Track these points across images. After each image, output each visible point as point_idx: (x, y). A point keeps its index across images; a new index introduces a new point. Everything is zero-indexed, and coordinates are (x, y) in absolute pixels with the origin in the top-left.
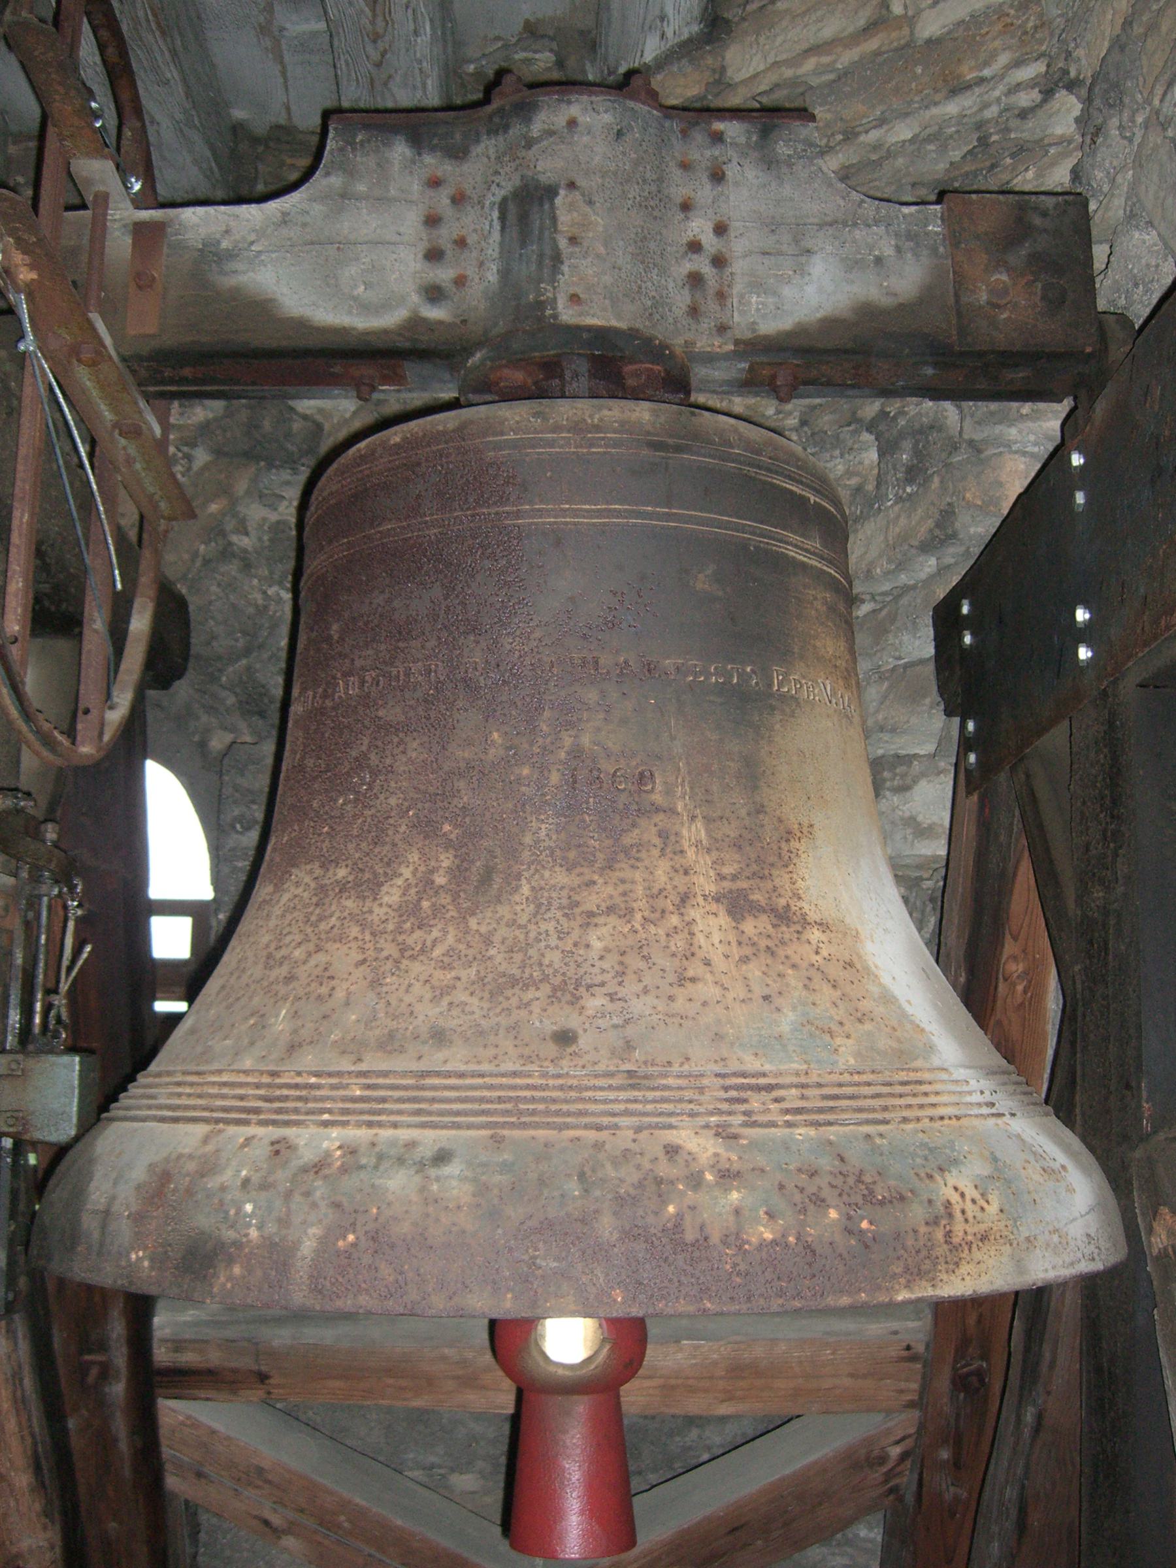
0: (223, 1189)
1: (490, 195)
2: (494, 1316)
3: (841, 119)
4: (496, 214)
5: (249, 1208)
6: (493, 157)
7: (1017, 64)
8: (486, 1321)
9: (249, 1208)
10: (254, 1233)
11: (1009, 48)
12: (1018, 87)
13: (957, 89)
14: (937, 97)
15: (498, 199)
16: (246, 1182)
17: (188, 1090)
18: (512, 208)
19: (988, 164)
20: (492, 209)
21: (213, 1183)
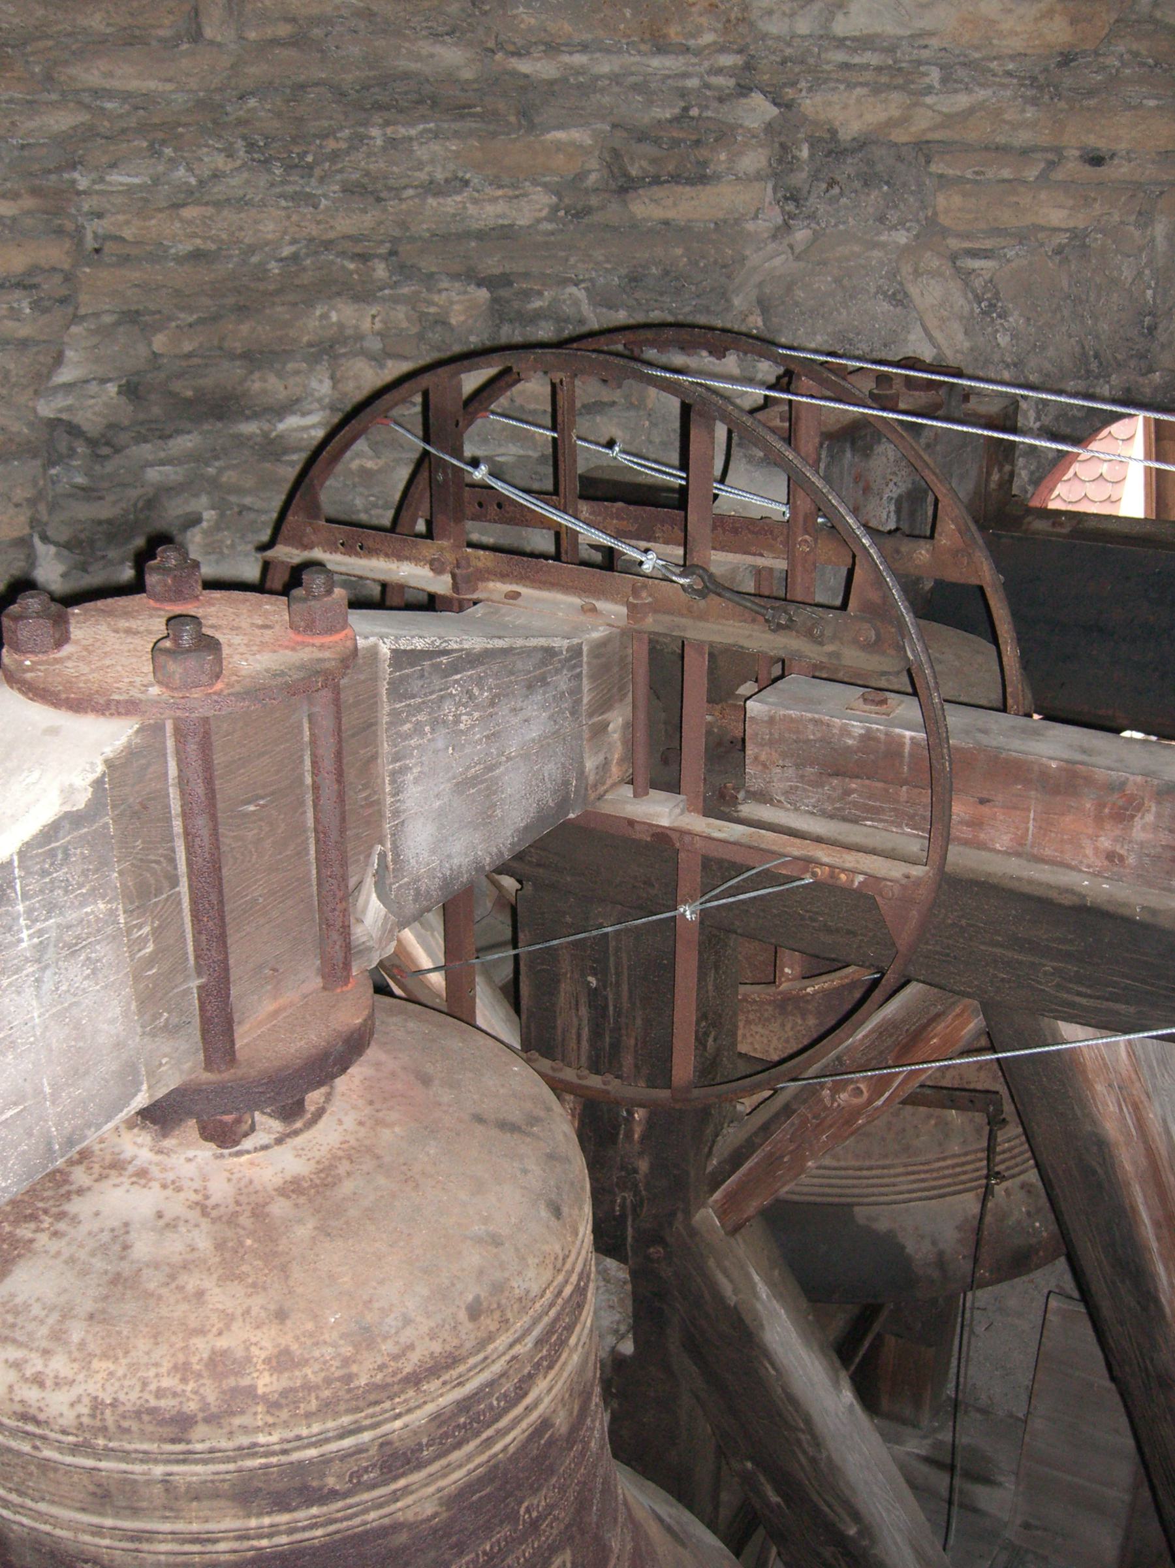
0: (1019, 1222)
1: (887, 490)
2: (371, 990)
3: (545, 30)
4: (892, 508)
5: (1037, 1224)
6: (892, 459)
7: (723, 49)
8: (377, 996)
9: (1037, 1224)
10: (1045, 1234)
11: (715, 31)
12: (719, 71)
13: (661, 47)
14: (643, 47)
15: (895, 495)
16: (1029, 1214)
17: (946, 1172)
18: (905, 505)
19: (694, 137)
20: (889, 502)
21: (1011, 1221)
